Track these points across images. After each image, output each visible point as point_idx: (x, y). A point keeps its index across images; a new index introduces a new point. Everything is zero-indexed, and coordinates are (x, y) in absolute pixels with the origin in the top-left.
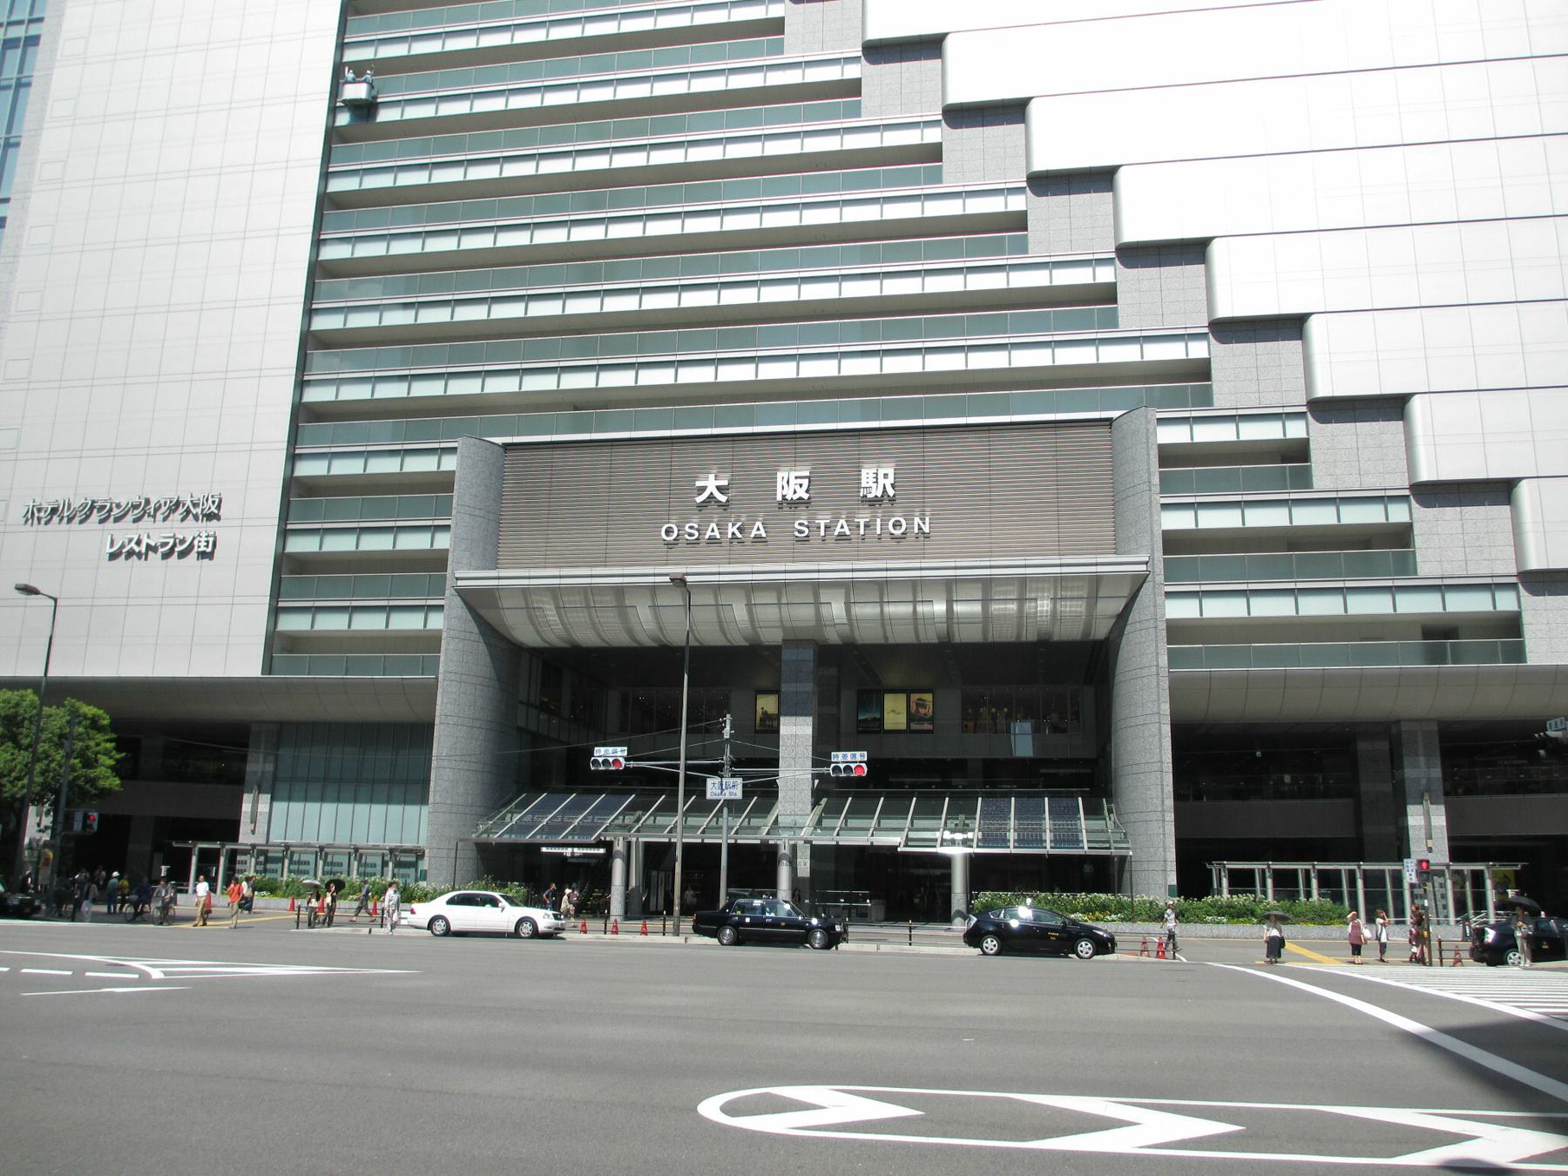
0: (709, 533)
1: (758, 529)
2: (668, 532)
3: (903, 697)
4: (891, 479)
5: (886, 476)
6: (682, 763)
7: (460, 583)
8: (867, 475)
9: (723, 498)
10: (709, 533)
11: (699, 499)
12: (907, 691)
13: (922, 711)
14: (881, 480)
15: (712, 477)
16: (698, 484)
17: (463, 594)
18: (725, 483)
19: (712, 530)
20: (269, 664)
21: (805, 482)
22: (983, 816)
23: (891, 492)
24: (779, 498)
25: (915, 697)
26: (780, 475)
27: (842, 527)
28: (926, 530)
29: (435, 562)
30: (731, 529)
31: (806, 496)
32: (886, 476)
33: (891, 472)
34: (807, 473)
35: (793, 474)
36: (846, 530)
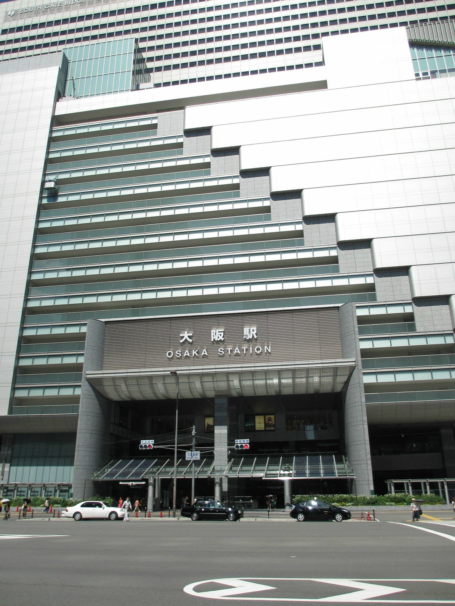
0: (185, 354)
1: (204, 352)
2: (170, 354)
3: (262, 417)
4: (255, 332)
5: (253, 330)
6: (176, 446)
7: (88, 376)
8: (246, 330)
9: (190, 341)
10: (185, 354)
11: (181, 341)
12: (264, 414)
13: (270, 422)
14: (252, 332)
15: (186, 332)
16: (181, 335)
17: (89, 380)
18: (191, 335)
19: (187, 353)
20: (11, 411)
21: (222, 334)
22: (296, 464)
23: (255, 337)
24: (212, 340)
25: (267, 417)
26: (212, 331)
27: (237, 350)
28: (270, 351)
29: (78, 368)
30: (194, 353)
31: (223, 339)
32: (253, 330)
33: (255, 329)
34: (223, 330)
35: (218, 331)
36: (239, 352)
